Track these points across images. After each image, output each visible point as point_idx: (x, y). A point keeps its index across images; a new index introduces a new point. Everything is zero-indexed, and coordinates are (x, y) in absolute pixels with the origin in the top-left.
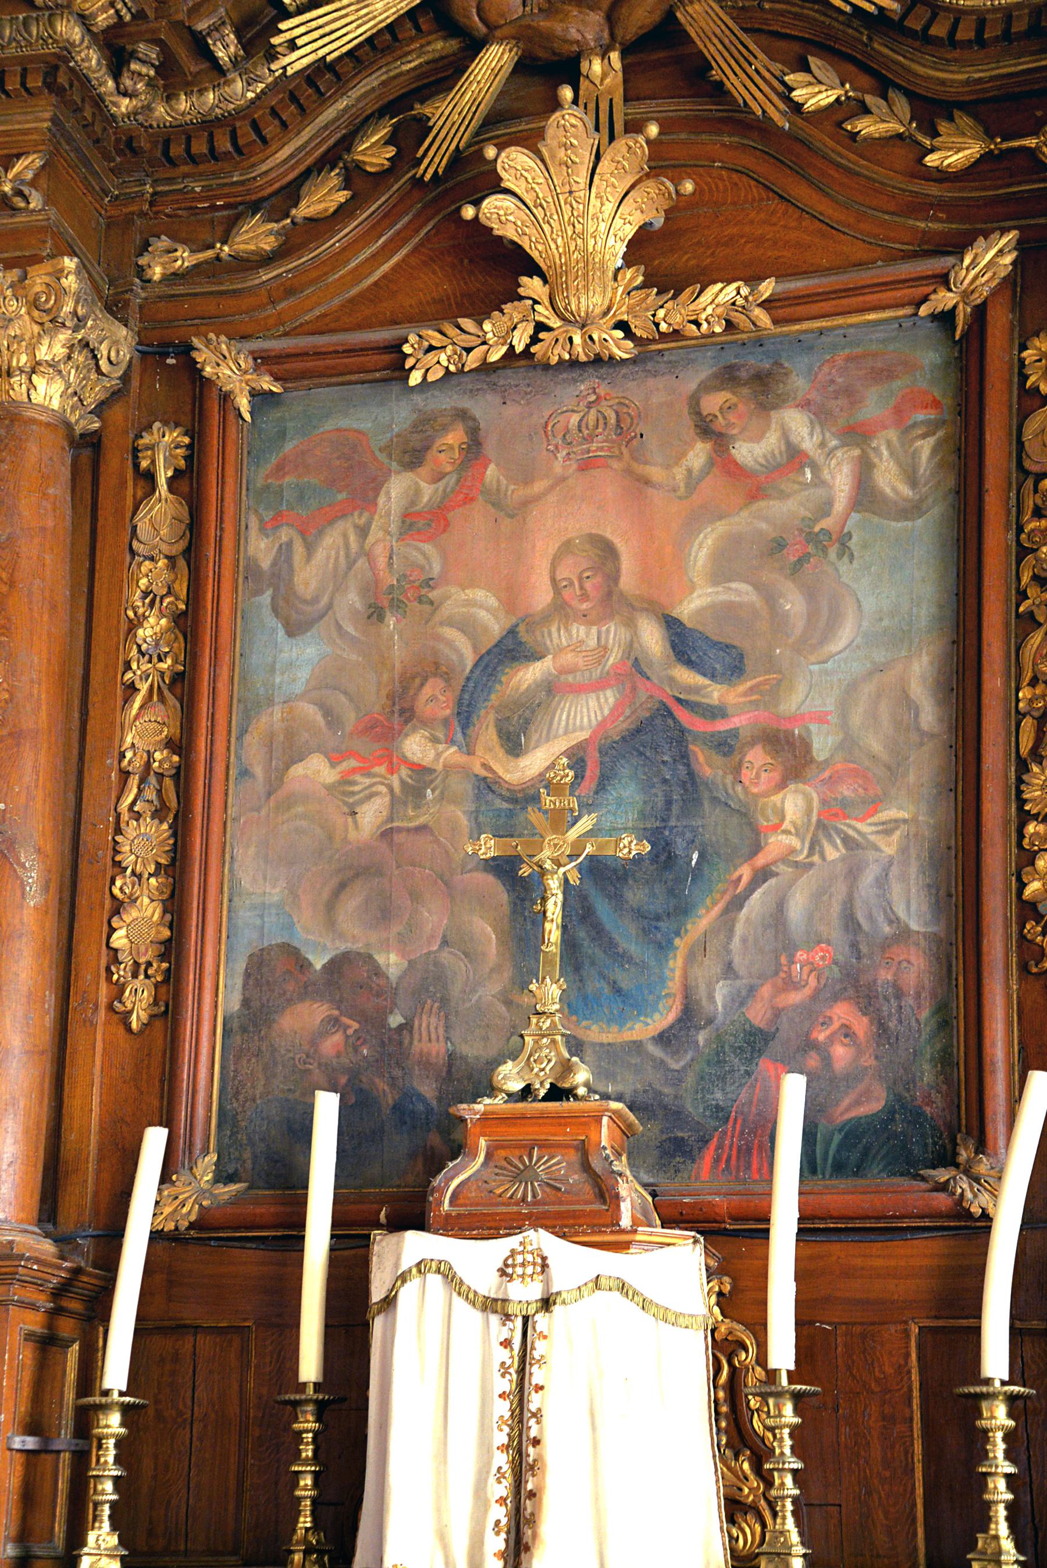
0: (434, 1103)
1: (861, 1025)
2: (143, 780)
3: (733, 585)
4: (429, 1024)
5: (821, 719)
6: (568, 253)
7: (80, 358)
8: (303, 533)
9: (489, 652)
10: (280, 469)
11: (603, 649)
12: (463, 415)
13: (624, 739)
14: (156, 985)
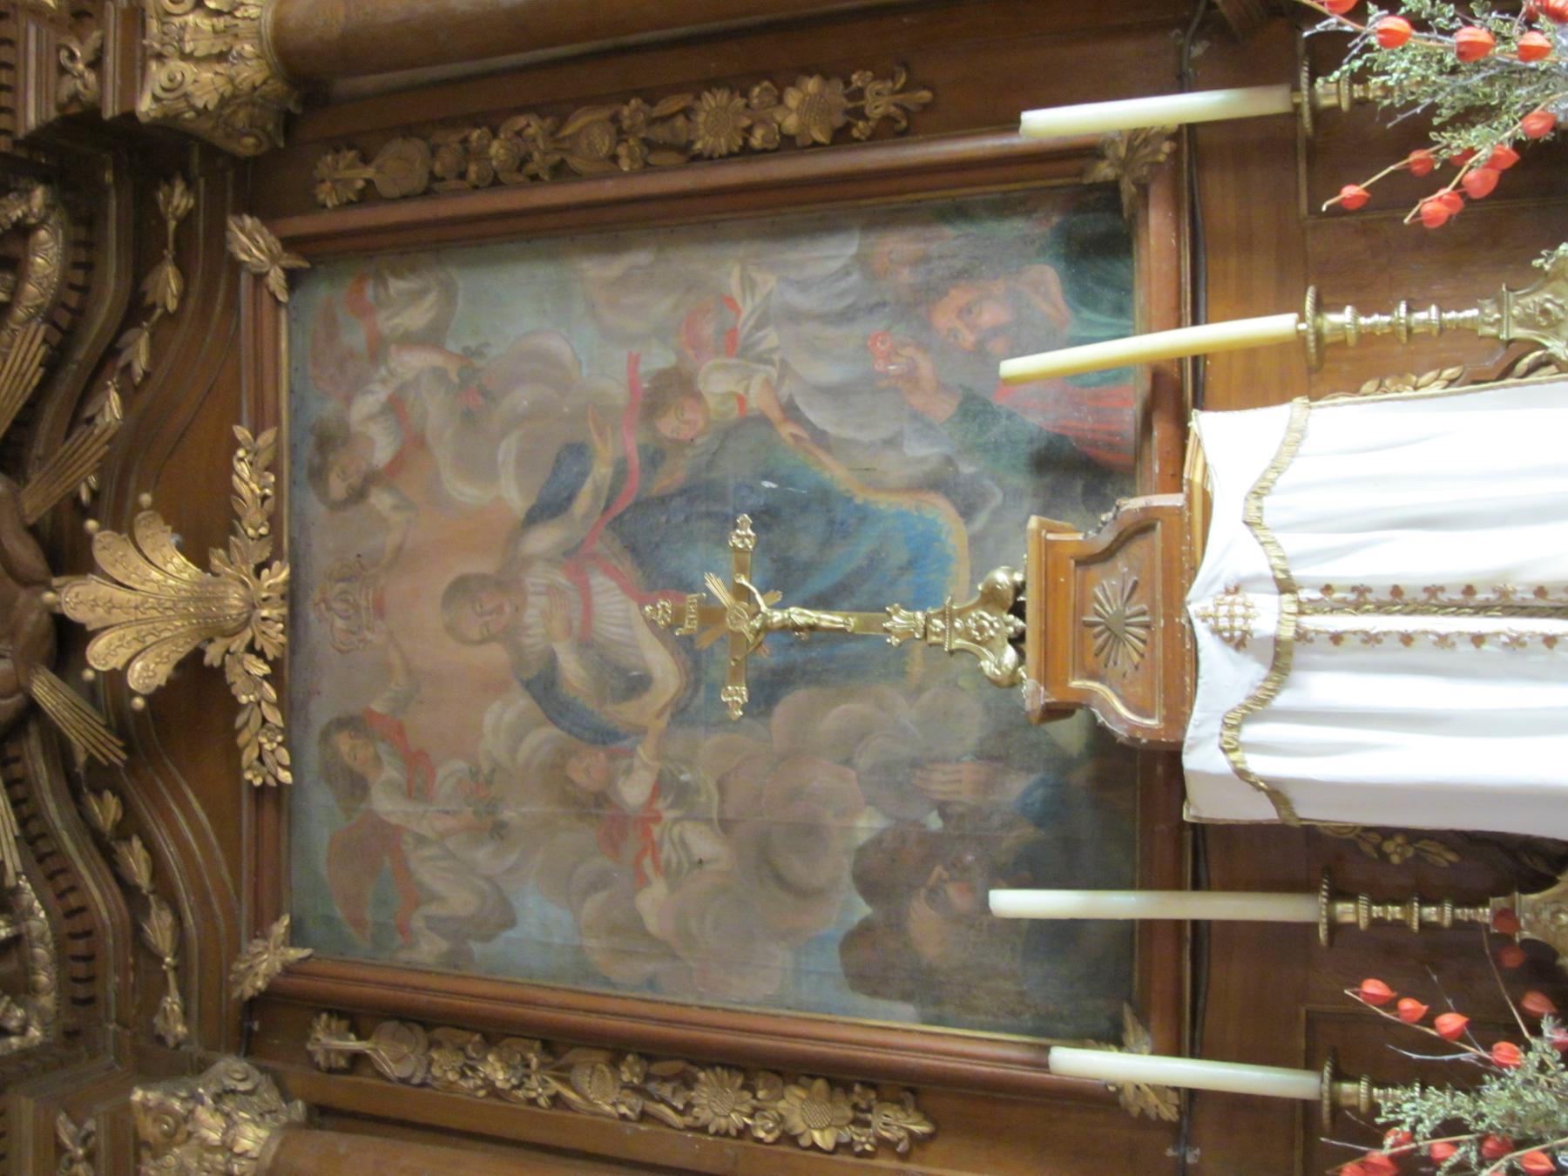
0: (1034, 778)
1: (959, 296)
2: (650, 1097)
3: (500, 458)
4: (941, 782)
5: (634, 361)
6: (189, 616)
7: (228, 1106)
8: (417, 904)
9: (545, 711)
10: (358, 923)
11: (551, 590)
12: (325, 736)
13: (641, 565)
14: (881, 1099)
